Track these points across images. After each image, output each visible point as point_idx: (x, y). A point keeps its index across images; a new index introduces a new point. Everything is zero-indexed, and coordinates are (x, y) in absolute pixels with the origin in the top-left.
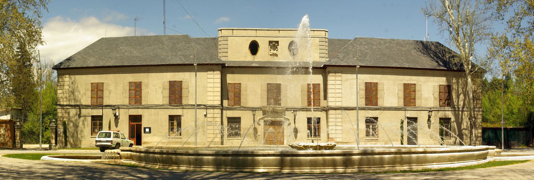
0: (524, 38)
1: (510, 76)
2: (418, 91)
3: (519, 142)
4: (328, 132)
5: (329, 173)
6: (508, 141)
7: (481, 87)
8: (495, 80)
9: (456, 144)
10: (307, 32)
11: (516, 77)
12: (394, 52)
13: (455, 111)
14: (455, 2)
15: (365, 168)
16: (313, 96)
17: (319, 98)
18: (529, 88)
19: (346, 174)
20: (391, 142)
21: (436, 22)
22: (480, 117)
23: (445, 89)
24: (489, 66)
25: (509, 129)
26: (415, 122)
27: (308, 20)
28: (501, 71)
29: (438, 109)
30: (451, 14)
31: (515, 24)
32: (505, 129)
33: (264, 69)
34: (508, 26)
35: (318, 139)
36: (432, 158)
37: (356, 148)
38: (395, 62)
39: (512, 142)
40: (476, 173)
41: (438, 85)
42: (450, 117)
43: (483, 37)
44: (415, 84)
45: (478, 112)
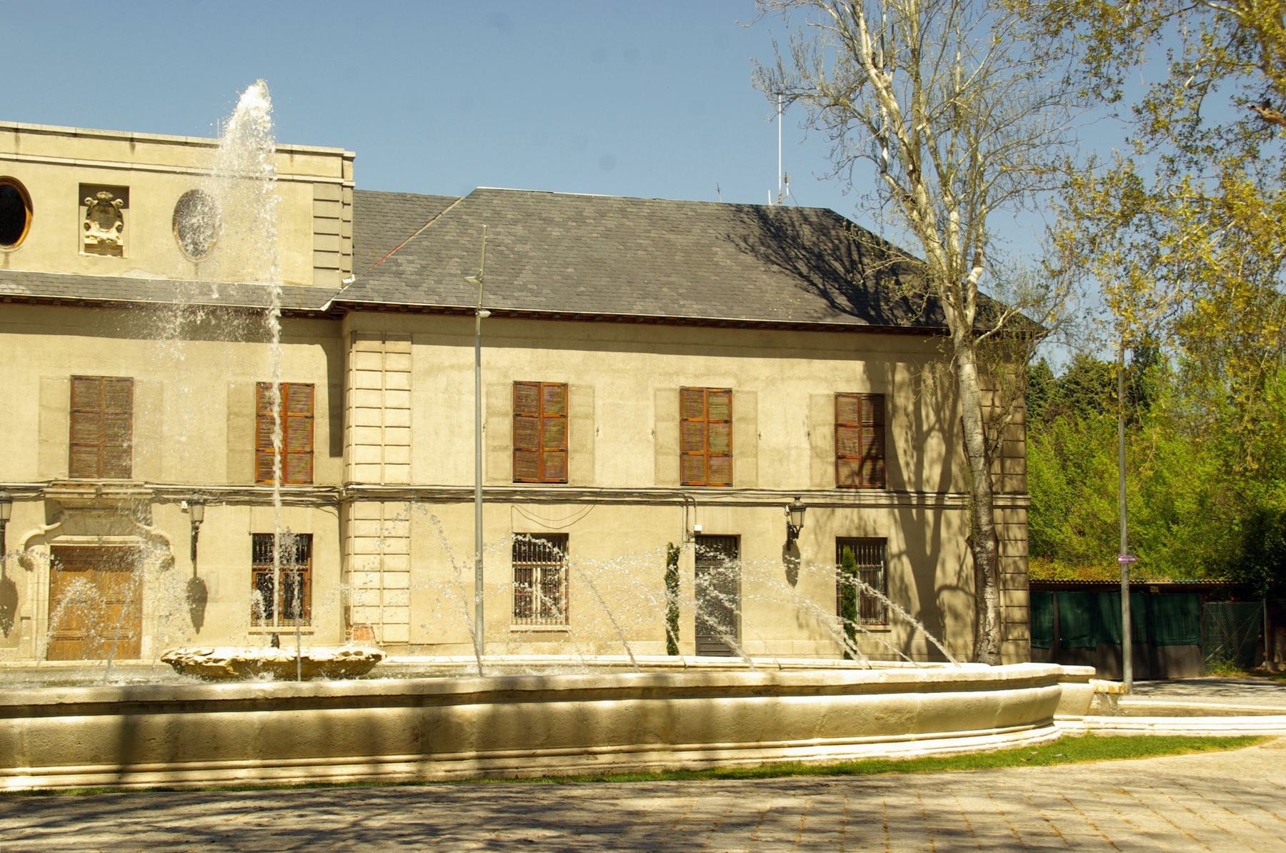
0: (1217, 176)
1: (1156, 350)
2: (743, 419)
3: (1203, 649)
4: (345, 597)
5: (349, 784)
6: (1153, 644)
7: (1021, 401)
8: (1083, 367)
9: (911, 656)
10: (262, 156)
11: (1182, 351)
12: (640, 252)
13: (905, 506)
14: (899, 37)
15: (510, 760)
16: (281, 437)
17: (308, 449)
18: (1247, 398)
19: (425, 789)
20: (625, 644)
21: (820, 124)
22: (1017, 533)
23: (859, 412)
24: (1055, 305)
25: (1154, 590)
26: (729, 555)
27: (265, 104)
28: (1112, 324)
29: (828, 501)
30: (886, 88)
31: (1175, 117)
32: (1134, 589)
33: (107, 313)
34: (1139, 126)
35: (302, 629)
36: (805, 713)
37: (469, 670)
38: (644, 296)
39: (1172, 650)
40: (1004, 789)
41: (828, 396)
42: (882, 533)
43: (1028, 180)
44: (728, 392)
45: (1008, 511)
